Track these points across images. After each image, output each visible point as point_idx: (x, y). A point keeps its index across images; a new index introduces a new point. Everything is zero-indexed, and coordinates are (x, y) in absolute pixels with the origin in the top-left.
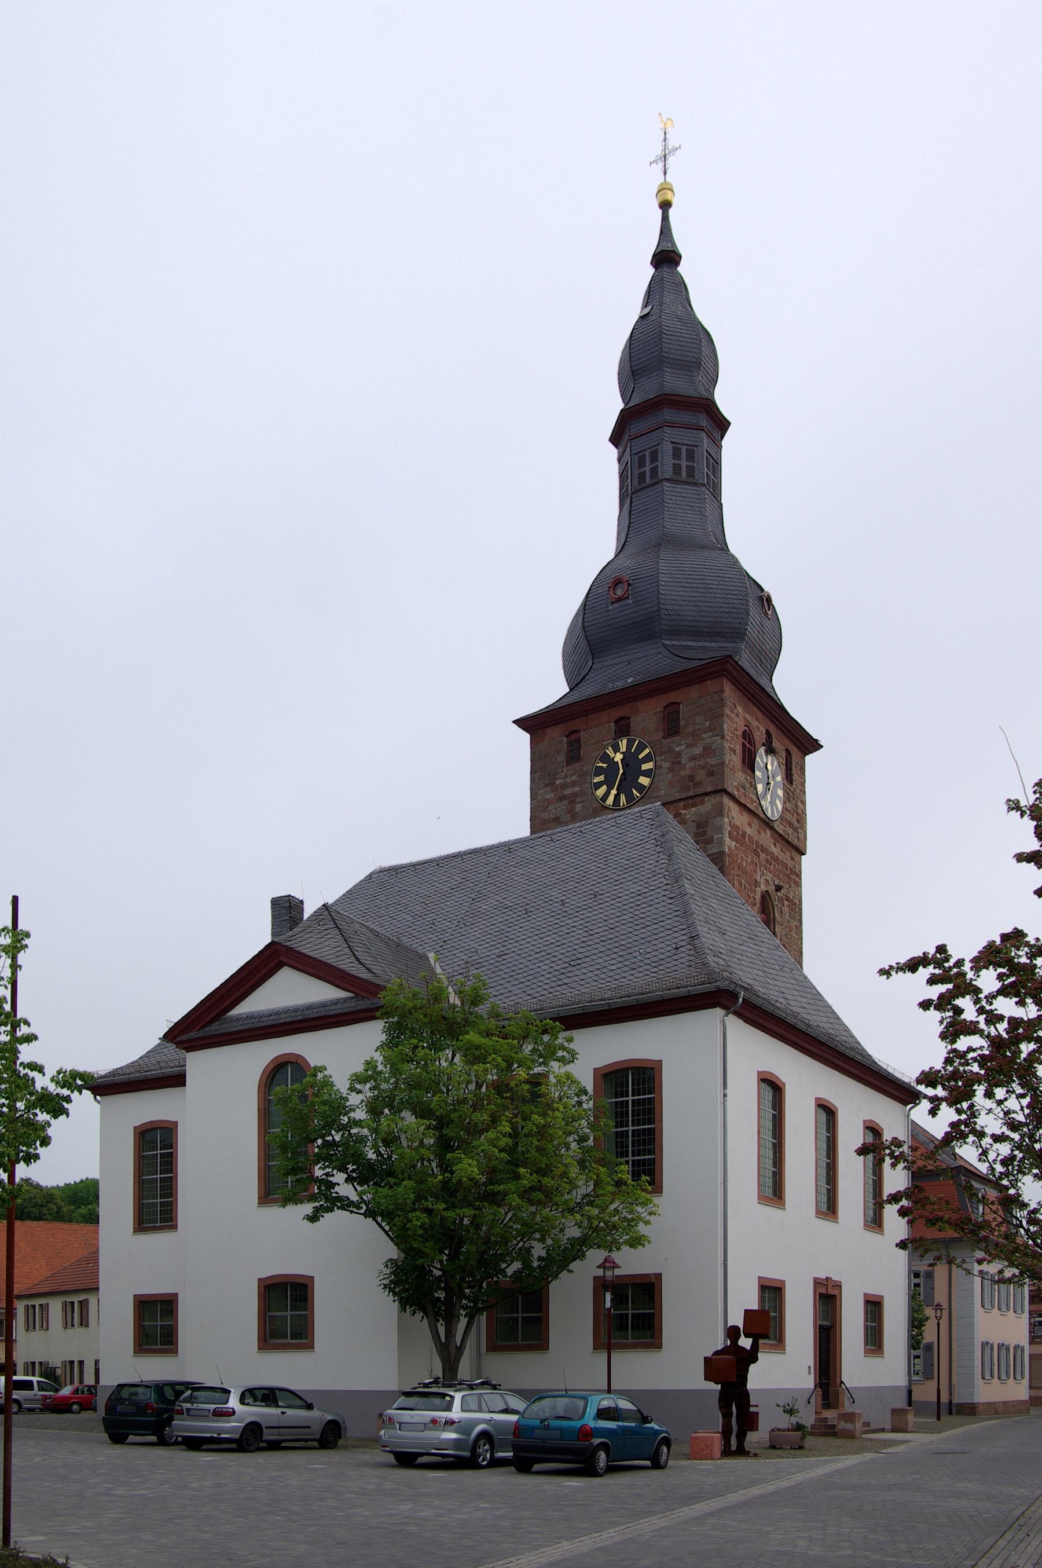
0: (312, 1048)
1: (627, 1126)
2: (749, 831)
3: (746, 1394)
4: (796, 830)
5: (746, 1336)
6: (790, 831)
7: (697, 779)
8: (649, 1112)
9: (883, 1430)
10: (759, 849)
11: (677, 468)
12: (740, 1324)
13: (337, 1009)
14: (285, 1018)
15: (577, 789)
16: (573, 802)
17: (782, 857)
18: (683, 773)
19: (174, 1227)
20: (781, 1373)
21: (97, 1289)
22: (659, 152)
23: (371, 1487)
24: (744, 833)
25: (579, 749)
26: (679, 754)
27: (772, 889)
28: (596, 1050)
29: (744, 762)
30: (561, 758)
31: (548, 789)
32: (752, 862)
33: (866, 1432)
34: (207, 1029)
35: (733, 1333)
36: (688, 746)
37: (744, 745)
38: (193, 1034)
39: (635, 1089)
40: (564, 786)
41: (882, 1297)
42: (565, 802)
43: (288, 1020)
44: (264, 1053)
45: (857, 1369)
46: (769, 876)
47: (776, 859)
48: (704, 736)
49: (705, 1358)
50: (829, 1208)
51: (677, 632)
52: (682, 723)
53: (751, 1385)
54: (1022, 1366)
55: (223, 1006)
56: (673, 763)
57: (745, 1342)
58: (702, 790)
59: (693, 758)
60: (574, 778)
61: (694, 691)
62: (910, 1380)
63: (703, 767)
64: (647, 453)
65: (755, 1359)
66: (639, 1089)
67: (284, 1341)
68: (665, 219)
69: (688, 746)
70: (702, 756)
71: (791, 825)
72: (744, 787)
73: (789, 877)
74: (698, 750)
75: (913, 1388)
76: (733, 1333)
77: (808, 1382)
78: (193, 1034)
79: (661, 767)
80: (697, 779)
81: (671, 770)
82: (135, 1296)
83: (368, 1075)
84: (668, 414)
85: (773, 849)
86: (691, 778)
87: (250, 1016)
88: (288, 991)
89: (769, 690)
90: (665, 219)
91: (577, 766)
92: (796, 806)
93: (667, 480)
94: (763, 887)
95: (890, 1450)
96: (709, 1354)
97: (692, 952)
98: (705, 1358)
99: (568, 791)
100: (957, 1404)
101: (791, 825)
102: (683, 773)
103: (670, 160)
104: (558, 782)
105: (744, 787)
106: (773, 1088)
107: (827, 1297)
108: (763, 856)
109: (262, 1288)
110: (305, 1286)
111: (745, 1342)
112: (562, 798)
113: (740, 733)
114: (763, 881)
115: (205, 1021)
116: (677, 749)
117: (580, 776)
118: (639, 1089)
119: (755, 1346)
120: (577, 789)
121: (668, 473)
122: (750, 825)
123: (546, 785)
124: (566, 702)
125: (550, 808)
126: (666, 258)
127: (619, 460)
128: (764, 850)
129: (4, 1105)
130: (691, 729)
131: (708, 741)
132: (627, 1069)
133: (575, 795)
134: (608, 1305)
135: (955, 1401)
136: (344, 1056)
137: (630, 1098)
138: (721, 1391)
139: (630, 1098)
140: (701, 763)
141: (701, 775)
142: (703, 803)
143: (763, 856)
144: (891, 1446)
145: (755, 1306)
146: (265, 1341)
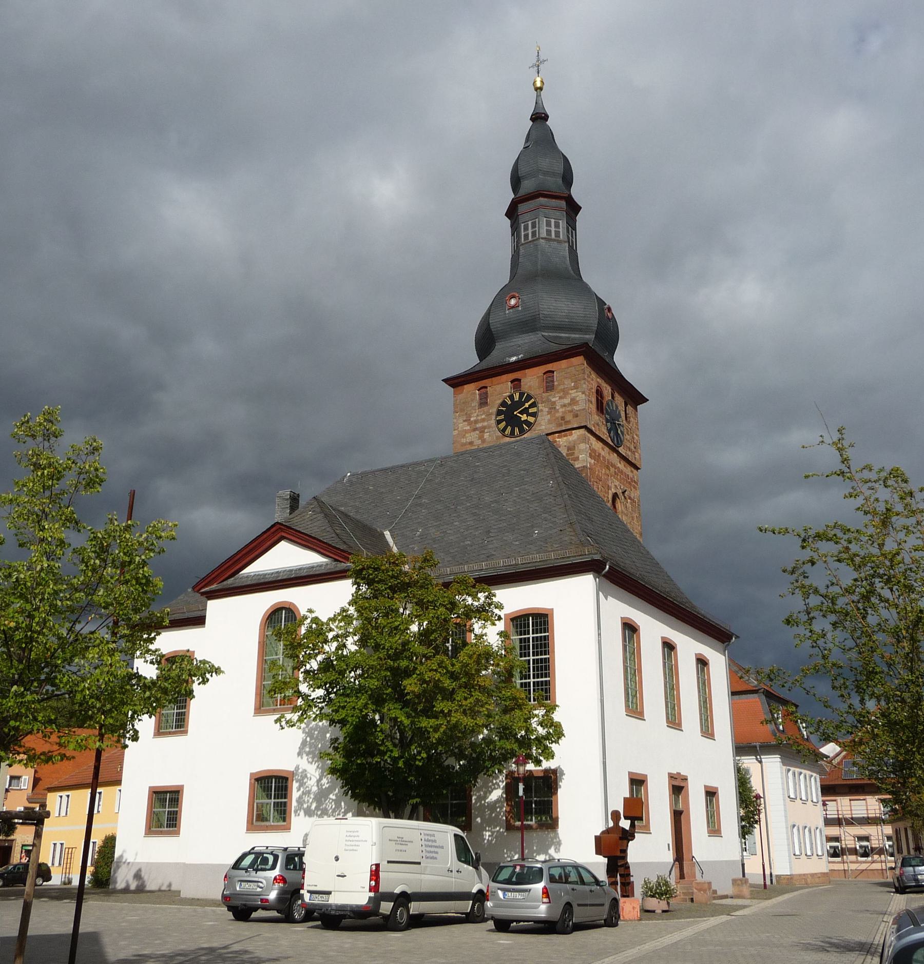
2: (603, 453)
3: (627, 867)
4: (633, 453)
5: (626, 818)
6: (630, 453)
8: (544, 646)
9: (726, 897)
10: (609, 465)
11: (549, 232)
15: (485, 424)
16: (483, 432)
17: (624, 470)
18: (557, 415)
20: (649, 852)
21: (118, 782)
23: (347, 946)
24: (600, 454)
26: (554, 402)
28: (514, 599)
30: (475, 404)
32: (605, 474)
33: (714, 898)
34: (225, 583)
35: (616, 816)
36: (560, 398)
39: (535, 627)
40: (476, 422)
41: (717, 788)
44: (261, 603)
45: (703, 847)
46: (617, 483)
47: (622, 472)
49: (596, 837)
50: (674, 721)
52: (556, 383)
57: (625, 824)
58: (570, 427)
59: (564, 406)
61: (564, 363)
62: (742, 856)
63: (570, 412)
64: (530, 223)
65: (633, 837)
67: (267, 823)
68: (538, 96)
69: (560, 398)
70: (570, 404)
71: (630, 449)
76: (616, 816)
81: (549, 413)
85: (619, 465)
86: (563, 418)
90: (538, 96)
91: (485, 409)
94: (614, 491)
95: (737, 913)
96: (598, 834)
98: (596, 837)
99: (479, 425)
101: (630, 449)
102: (557, 415)
103: (541, 67)
105: (598, 424)
109: (253, 781)
110: (287, 779)
111: (625, 824)
112: (475, 430)
113: (594, 390)
116: (553, 400)
119: (633, 825)
120: (485, 424)
122: (603, 449)
124: (477, 369)
126: (539, 117)
128: (613, 466)
129: (3, 652)
130: (562, 387)
132: (528, 615)
133: (484, 428)
134: (521, 793)
136: (329, 600)
139: (531, 636)
140: (569, 409)
141: (569, 417)
143: (612, 469)
144: (737, 910)
145: (628, 796)
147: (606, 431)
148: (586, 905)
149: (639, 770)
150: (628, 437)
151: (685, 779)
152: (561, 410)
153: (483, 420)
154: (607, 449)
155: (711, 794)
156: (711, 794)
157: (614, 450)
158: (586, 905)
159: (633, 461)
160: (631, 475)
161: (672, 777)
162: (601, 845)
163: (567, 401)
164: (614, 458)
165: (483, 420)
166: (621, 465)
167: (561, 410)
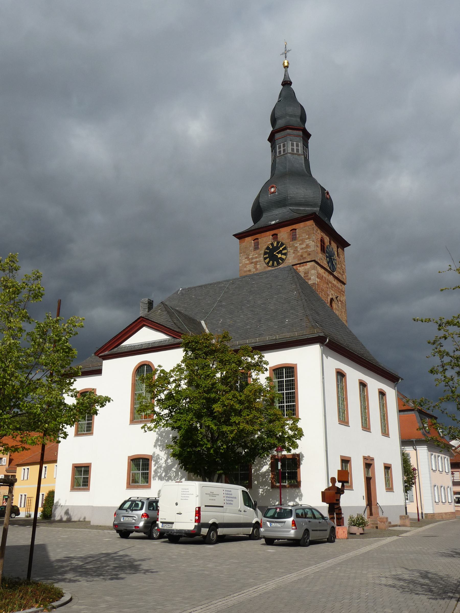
0: (155, 359)
1: (283, 391)
2: (324, 275)
3: (340, 509)
4: (342, 275)
5: (339, 481)
6: (340, 275)
7: (304, 256)
8: (292, 385)
11: (293, 150)
12: (336, 477)
13: (167, 343)
14: (156, 345)
15: (258, 260)
16: (256, 264)
17: (337, 285)
19: (92, 434)
20: (353, 500)
22: (283, 51)
23: (183, 552)
24: (323, 276)
25: (258, 245)
26: (297, 247)
27: (334, 297)
28: (274, 359)
29: (321, 250)
30: (252, 248)
31: (246, 259)
33: (390, 527)
34: (112, 351)
35: (333, 480)
36: (300, 244)
37: (321, 244)
38: (106, 353)
40: (252, 258)
42: (253, 264)
43: (146, 347)
44: (134, 361)
45: (383, 498)
46: (333, 292)
47: (335, 286)
48: (306, 241)
50: (366, 427)
51: (291, 205)
52: (297, 236)
53: (342, 504)
54: (441, 496)
55: (119, 342)
56: (295, 250)
57: (339, 485)
58: (306, 261)
59: (302, 249)
60: (256, 255)
61: (302, 225)
62: (406, 503)
63: (306, 252)
65: (343, 492)
66: (288, 376)
68: (286, 71)
70: (305, 248)
71: (340, 273)
72: (322, 259)
73: (340, 293)
74: (304, 246)
75: (407, 506)
76: (333, 480)
77: (364, 503)
78: (106, 353)
79: (290, 252)
80: (304, 256)
81: (294, 253)
82: (73, 464)
83: (178, 368)
84: (288, 131)
86: (302, 256)
87: (130, 346)
88: (146, 336)
89: (329, 225)
90: (286, 71)
91: (258, 251)
92: (342, 266)
93: (289, 153)
94: (331, 297)
96: (323, 490)
97: (307, 321)
99: (254, 260)
100: (425, 514)
101: (340, 273)
102: (299, 254)
103: (288, 54)
104: (250, 257)
105: (322, 259)
106: (341, 375)
107: (368, 464)
108: (330, 285)
109: (130, 461)
111: (339, 485)
112: (252, 263)
113: (319, 240)
114: (330, 294)
115: (113, 347)
116: (296, 245)
117: (258, 255)
118: (288, 376)
119: (343, 486)
120: (258, 260)
121: (290, 151)
122: (325, 273)
123: (246, 258)
125: (247, 266)
127: (271, 147)
128: (331, 282)
130: (301, 238)
131: (307, 243)
133: (257, 262)
134: (279, 468)
135: (424, 512)
137: (285, 379)
138: (329, 508)
139: (285, 379)
140: (305, 250)
142: (306, 265)
143: (330, 285)
146: (130, 484)
147: (326, 263)
148: (317, 530)
149: (346, 454)
150: (339, 266)
151: (373, 459)
152: (300, 251)
153: (256, 258)
154: (327, 273)
155: (387, 468)
156: (387, 468)
157: (331, 273)
158: (317, 530)
159: (342, 280)
160: (341, 287)
161: (365, 458)
162: (325, 496)
163: (304, 246)
164: (331, 278)
165: (256, 258)
166: (335, 282)
167: (300, 251)
